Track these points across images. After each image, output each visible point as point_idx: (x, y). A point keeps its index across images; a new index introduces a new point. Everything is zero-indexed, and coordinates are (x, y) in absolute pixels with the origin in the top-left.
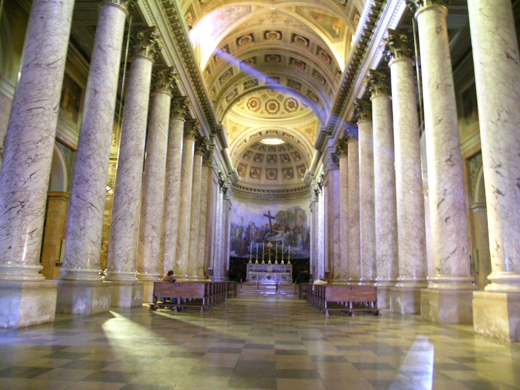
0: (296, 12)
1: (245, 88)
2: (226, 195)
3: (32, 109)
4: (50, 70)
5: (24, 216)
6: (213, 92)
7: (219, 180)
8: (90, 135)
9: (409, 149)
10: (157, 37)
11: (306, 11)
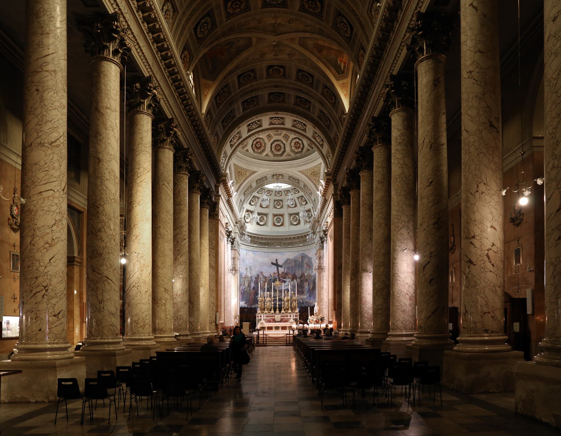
0: (300, 45)
1: (249, 131)
2: (234, 245)
3: (43, 192)
4: (54, 148)
5: (49, 300)
8: (98, 207)
10: (155, 89)
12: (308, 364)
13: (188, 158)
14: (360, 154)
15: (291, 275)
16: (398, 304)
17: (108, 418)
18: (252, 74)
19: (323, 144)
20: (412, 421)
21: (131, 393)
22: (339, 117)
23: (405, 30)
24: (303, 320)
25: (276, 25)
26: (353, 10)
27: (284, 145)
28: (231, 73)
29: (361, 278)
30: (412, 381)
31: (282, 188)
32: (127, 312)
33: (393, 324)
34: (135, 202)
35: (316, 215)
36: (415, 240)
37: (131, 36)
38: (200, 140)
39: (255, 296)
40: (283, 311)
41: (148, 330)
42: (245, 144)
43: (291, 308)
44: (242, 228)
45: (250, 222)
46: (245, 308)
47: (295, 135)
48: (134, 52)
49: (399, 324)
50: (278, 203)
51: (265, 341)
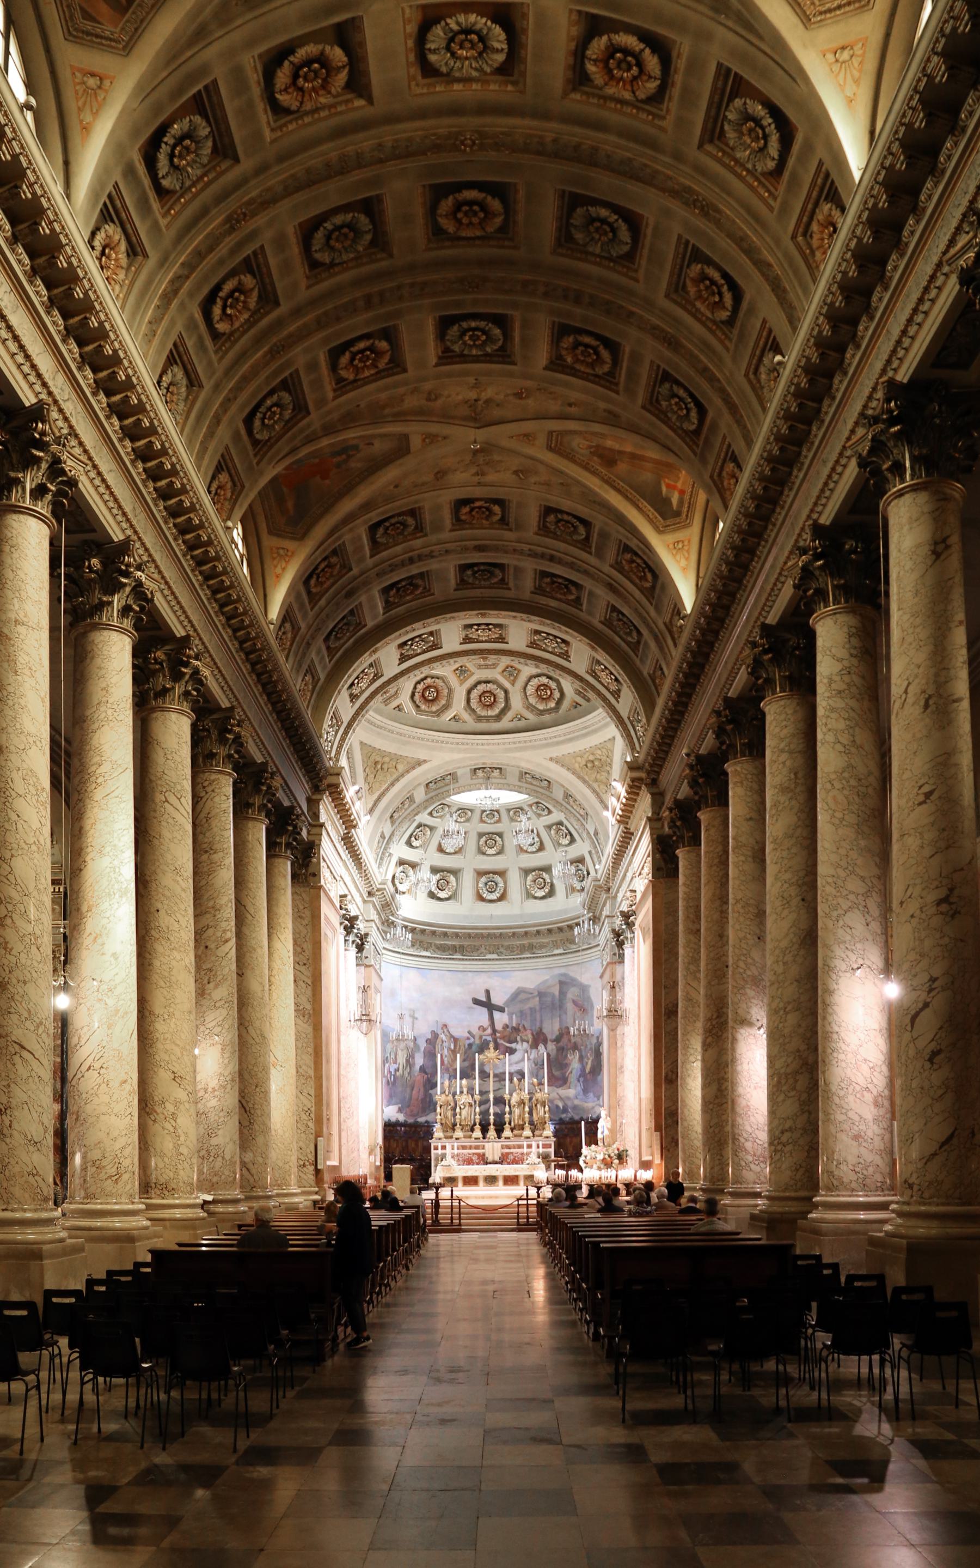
0: (550, 448)
1: (403, 659)
2: (365, 953)
7: (344, 916)
9: (854, 855)
10: (139, 568)
11: (579, 445)
12: (580, 1286)
13: (230, 731)
14: (726, 716)
15: (529, 1032)
16: (840, 1117)
17: (20, 1436)
18: (410, 521)
19: (619, 690)
20: (892, 1467)
21: (82, 1368)
22: (665, 624)
23: (854, 419)
24: (567, 1158)
25: (480, 403)
26: (706, 369)
27: (506, 692)
28: (349, 519)
29: (732, 1044)
30: (888, 1344)
31: (501, 801)
32: (71, 1137)
33: (830, 1173)
34: (90, 849)
35: (600, 872)
36: (887, 941)
37: (77, 451)
38: (264, 686)
39: (426, 1091)
40: (507, 1133)
41: (128, 1187)
42: (392, 691)
43: (531, 1123)
44: (387, 907)
45: (409, 891)
46: (397, 1124)
47: (537, 667)
48: (85, 486)
49: (846, 1173)
51: (456, 1210)
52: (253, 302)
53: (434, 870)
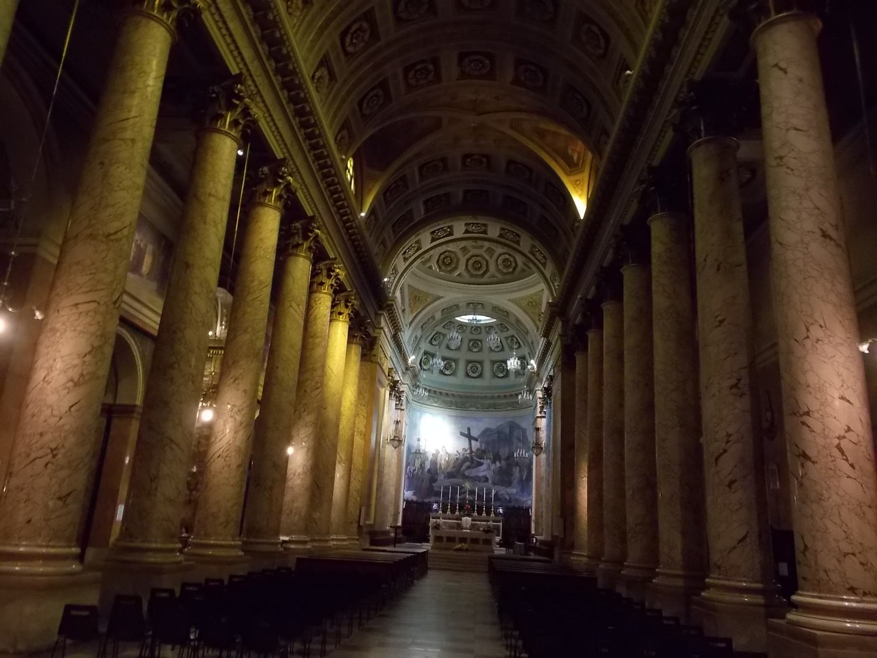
0: (512, 127)
1: (433, 240)
3: (79, 304)
6: (382, 247)
15: (491, 454)
46: (412, 501)
47: (503, 248)
50: (476, 344)
52: (367, 36)
53: (444, 359)
